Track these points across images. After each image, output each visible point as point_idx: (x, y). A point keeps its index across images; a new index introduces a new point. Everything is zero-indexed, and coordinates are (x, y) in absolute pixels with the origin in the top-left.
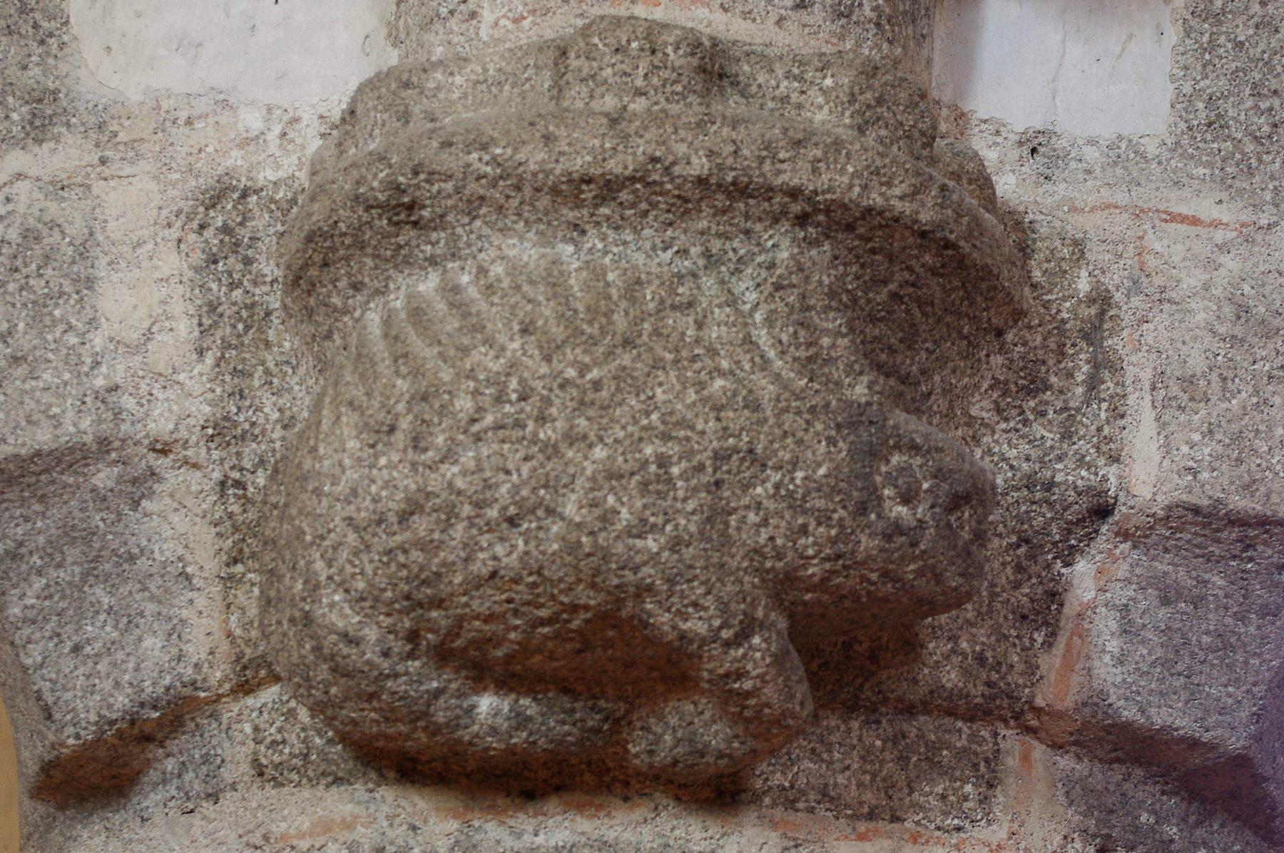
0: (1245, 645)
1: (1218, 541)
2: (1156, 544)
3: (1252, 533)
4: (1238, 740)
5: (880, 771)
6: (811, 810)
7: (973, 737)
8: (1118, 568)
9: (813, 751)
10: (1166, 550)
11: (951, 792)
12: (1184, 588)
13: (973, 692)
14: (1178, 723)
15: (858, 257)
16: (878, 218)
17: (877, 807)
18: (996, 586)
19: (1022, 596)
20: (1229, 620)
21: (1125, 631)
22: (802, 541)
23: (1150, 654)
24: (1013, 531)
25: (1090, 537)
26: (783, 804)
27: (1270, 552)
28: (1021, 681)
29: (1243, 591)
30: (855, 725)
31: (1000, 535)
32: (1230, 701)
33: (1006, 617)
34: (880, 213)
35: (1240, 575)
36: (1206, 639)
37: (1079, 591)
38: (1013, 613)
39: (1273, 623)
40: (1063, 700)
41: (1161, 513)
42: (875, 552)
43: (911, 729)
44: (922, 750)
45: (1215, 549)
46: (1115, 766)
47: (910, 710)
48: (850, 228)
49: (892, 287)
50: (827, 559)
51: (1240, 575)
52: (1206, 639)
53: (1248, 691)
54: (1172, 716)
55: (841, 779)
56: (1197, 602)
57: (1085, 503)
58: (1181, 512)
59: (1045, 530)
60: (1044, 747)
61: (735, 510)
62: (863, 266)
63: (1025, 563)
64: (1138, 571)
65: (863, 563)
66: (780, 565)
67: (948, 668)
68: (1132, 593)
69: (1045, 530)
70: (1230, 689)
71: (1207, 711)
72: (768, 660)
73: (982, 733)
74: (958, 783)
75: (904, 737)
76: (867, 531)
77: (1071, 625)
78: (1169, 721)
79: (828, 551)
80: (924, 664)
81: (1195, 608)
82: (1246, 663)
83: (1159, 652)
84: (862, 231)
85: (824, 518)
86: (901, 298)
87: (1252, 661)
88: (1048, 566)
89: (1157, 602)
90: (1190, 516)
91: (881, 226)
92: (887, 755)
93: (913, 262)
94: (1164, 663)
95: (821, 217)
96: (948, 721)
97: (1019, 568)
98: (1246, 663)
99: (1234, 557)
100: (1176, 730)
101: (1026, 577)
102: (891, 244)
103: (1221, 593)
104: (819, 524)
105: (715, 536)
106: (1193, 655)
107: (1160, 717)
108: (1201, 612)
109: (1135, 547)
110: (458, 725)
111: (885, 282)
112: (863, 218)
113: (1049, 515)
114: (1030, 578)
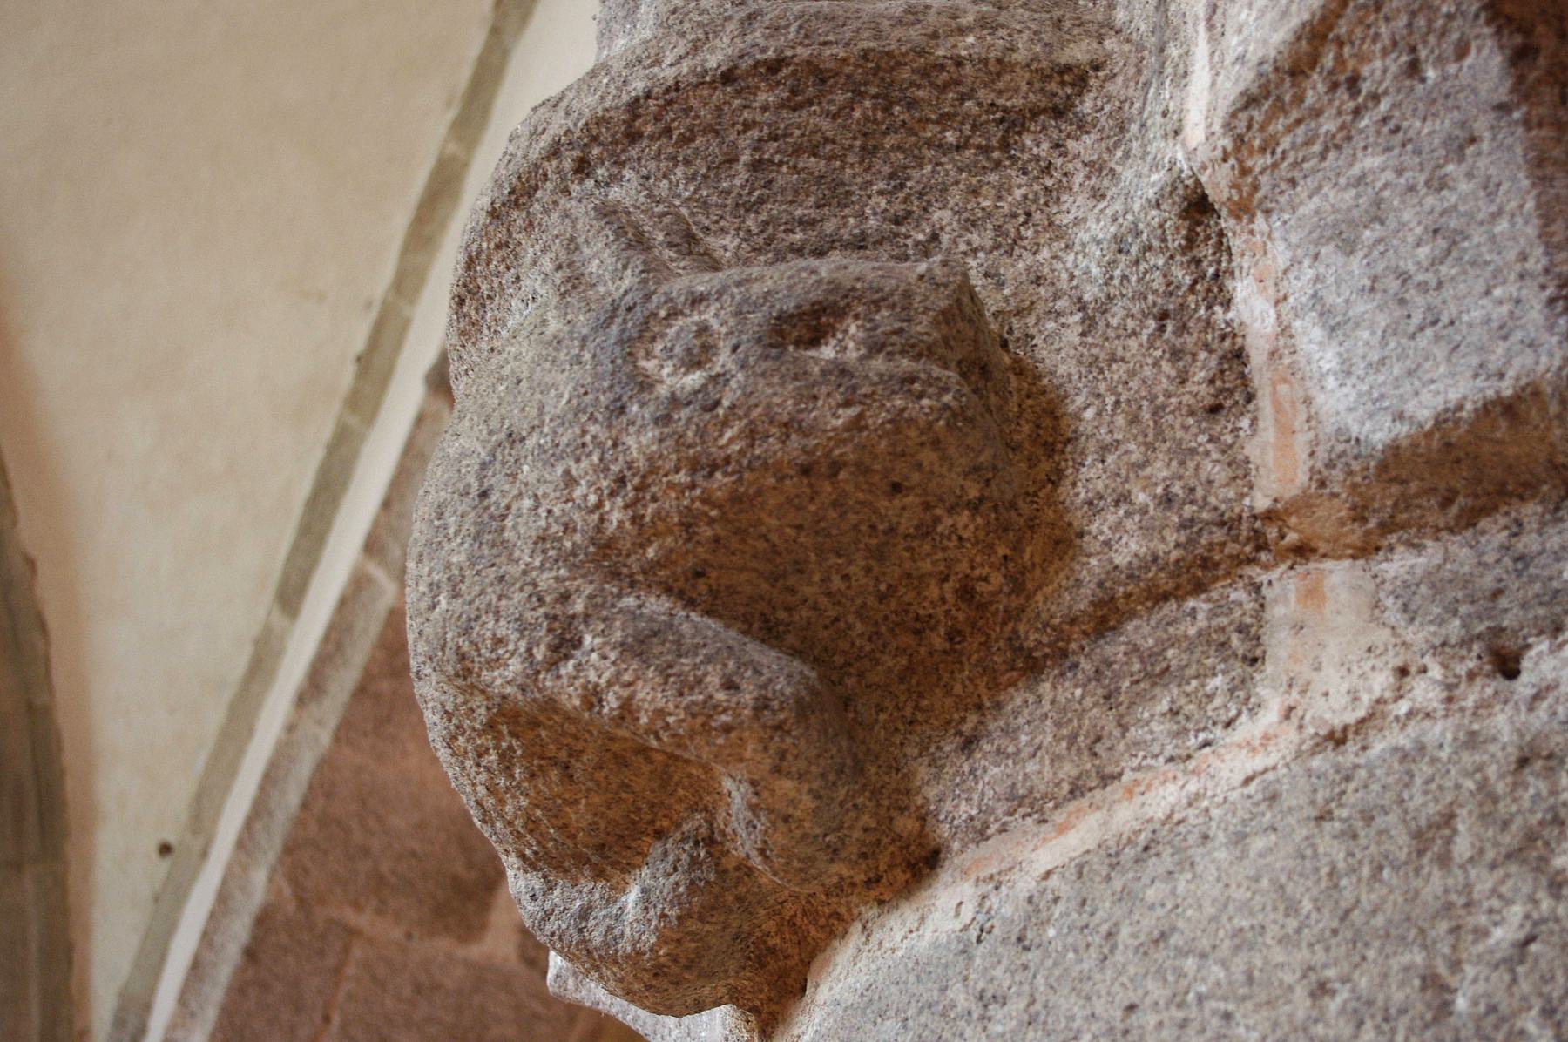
0: (1470, 216)
1: (1317, 113)
2: (1275, 186)
3: (1328, 60)
4: (1551, 355)
5: (1080, 727)
6: (1003, 829)
7: (1219, 609)
8: (1274, 257)
9: (999, 751)
10: (1293, 183)
11: (1183, 701)
12: (1349, 210)
13: (1162, 548)
14: (1454, 396)
15: (674, 158)
16: (651, 102)
17: (1078, 778)
18: (1157, 397)
19: (1199, 387)
20: (1430, 201)
21: (1333, 329)
22: (578, 492)
23: (1373, 333)
24: (1146, 316)
25: (1222, 247)
26: (973, 841)
27: (1378, 64)
28: (1231, 495)
29: (1409, 147)
30: (1045, 688)
31: (1134, 333)
32: (1505, 309)
33: (1186, 428)
34: (648, 96)
35: (1385, 130)
36: (1424, 252)
37: (1257, 325)
38: (1192, 413)
39: (1479, 154)
40: (1292, 481)
41: (1227, 142)
42: (654, 448)
43: (1114, 648)
44: (1137, 666)
45: (1328, 125)
46: (1483, 523)
47: (1107, 616)
48: (633, 137)
49: (745, 157)
50: (612, 494)
51: (1385, 130)
52: (1424, 252)
53: (1522, 277)
54: (1445, 388)
55: (1031, 767)
56: (1377, 217)
57: (1171, 211)
58: (1243, 116)
59: (1171, 288)
60: (1347, 563)
61: (508, 507)
62: (687, 162)
63: (1178, 342)
64: (1294, 239)
65: (653, 470)
66: (578, 538)
67: (1124, 540)
68: (1310, 273)
69: (1171, 288)
70: (1497, 292)
71: (1481, 349)
72: (613, 656)
73: (1233, 596)
74: (1194, 683)
75: (1110, 665)
76: (632, 430)
77: (1267, 375)
78: (1439, 403)
79: (605, 484)
80: (1089, 555)
81: (1382, 223)
82: (1492, 239)
83: (1383, 320)
84: (649, 129)
85: (579, 450)
86: (771, 161)
87: (1498, 229)
88: (1208, 324)
89: (1341, 259)
90: (1255, 113)
91: (663, 107)
92: (1088, 702)
93: (746, 114)
94: (1392, 330)
95: (596, 151)
96: (1170, 608)
97: (1176, 354)
98: (1492, 239)
99: (1357, 112)
100: (1460, 407)
101: (1189, 358)
102: (697, 117)
103: (1389, 175)
104: (578, 460)
105: (486, 552)
106: (1423, 287)
107: (1424, 408)
108: (1392, 223)
109: (1268, 212)
110: (615, 939)
111: (733, 160)
112: (636, 116)
113: (1161, 262)
114: (1194, 355)
